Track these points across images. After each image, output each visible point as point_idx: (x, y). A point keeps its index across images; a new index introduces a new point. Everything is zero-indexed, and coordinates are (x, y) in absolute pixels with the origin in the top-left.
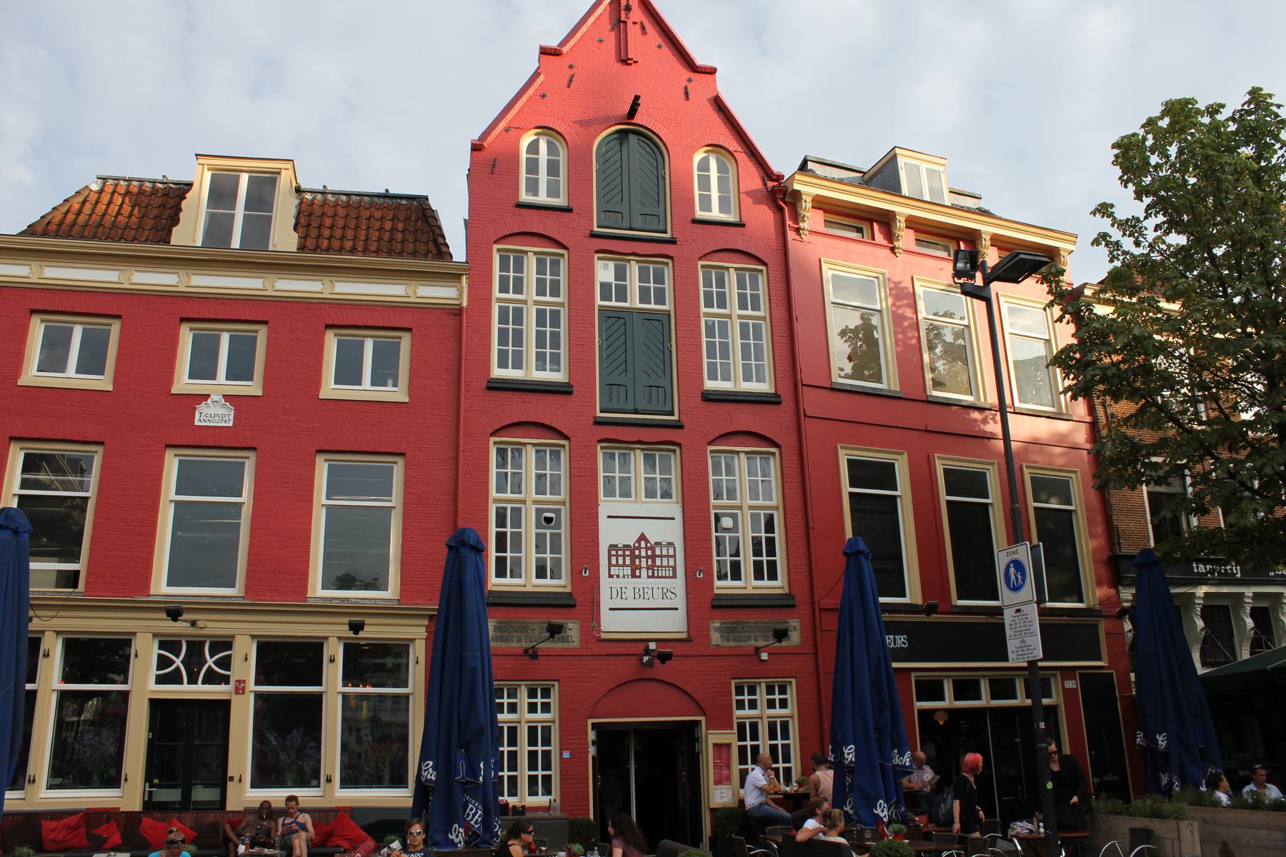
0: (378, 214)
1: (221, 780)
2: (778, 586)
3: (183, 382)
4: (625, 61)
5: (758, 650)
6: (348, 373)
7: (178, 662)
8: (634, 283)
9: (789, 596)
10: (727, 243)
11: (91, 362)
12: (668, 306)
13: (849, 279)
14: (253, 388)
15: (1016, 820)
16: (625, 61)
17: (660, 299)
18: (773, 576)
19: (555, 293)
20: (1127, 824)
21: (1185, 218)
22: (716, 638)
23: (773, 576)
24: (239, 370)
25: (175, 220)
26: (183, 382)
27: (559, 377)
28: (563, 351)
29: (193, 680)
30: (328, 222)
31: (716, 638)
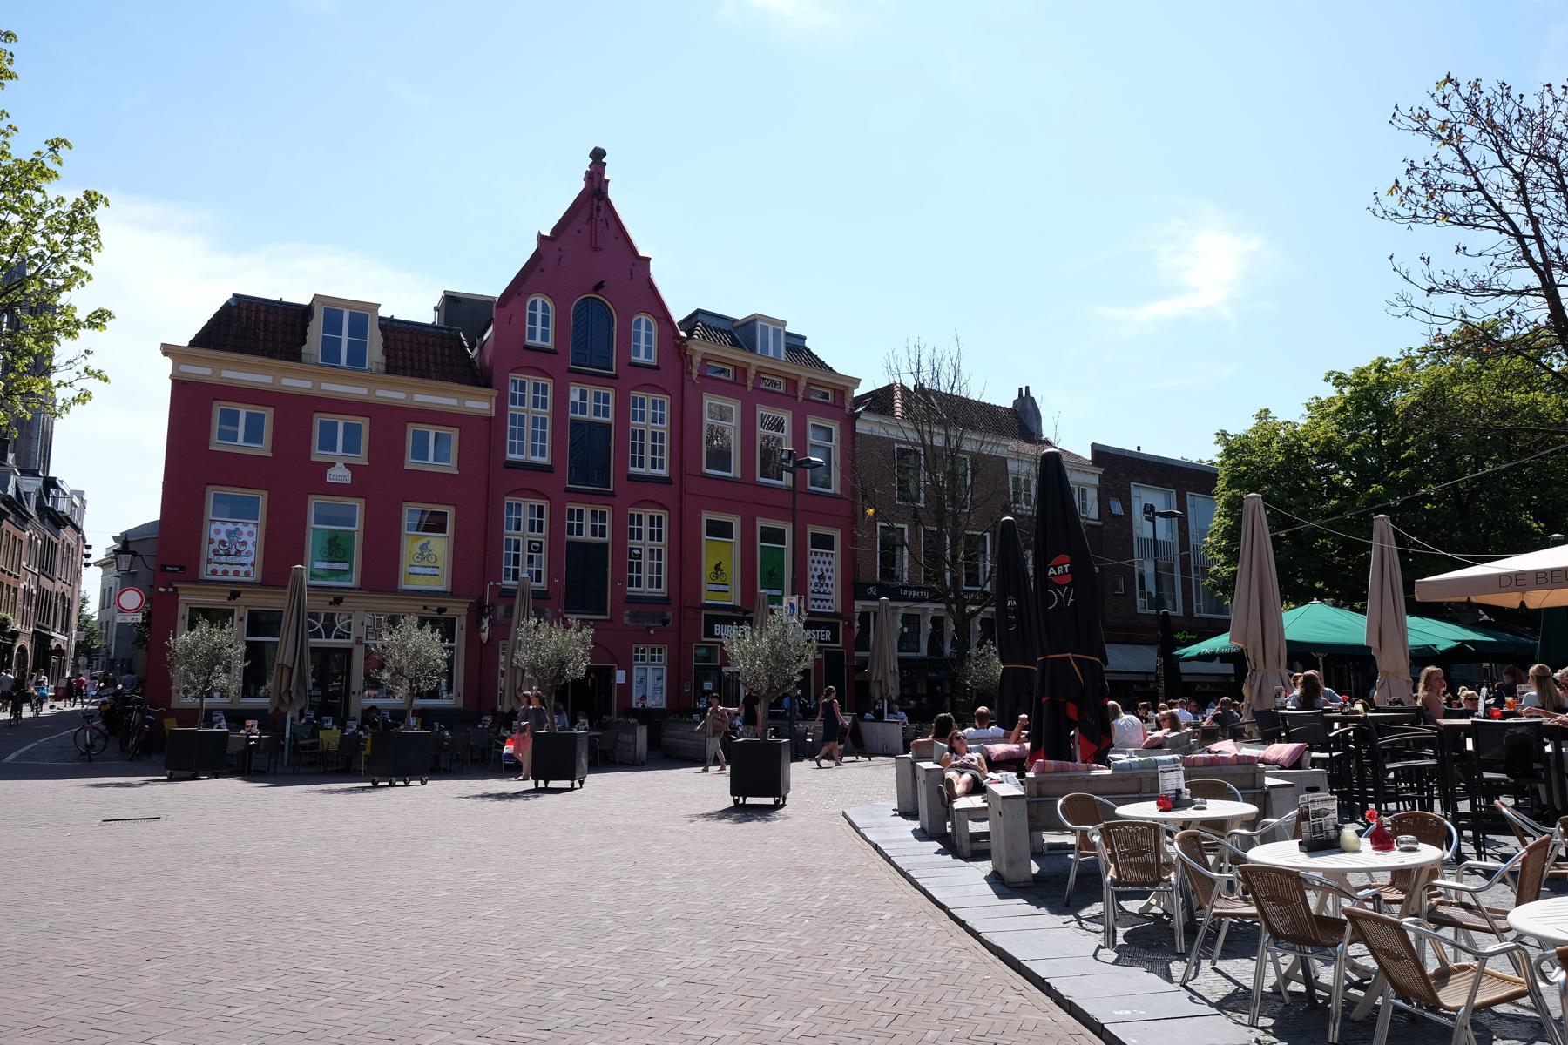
0: (430, 341)
1: (609, 713)
2: (662, 591)
3: (318, 455)
4: (596, 249)
5: (649, 628)
6: (421, 453)
7: (319, 625)
8: (590, 402)
9: (667, 598)
10: (647, 377)
11: (253, 434)
12: (610, 419)
13: (721, 416)
14: (361, 458)
15: (432, 326)
16: (596, 249)
17: (606, 415)
18: (659, 586)
19: (544, 407)
20: (397, 701)
21: (871, 511)
22: (626, 620)
23: (542, 455)
24: (351, 446)
25: (304, 342)
26: (318, 455)
27: (546, 460)
28: (548, 445)
29: (328, 637)
30: (399, 345)
31: (626, 620)
